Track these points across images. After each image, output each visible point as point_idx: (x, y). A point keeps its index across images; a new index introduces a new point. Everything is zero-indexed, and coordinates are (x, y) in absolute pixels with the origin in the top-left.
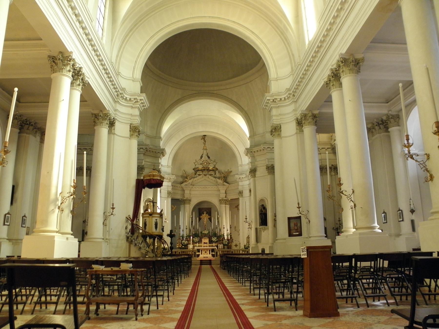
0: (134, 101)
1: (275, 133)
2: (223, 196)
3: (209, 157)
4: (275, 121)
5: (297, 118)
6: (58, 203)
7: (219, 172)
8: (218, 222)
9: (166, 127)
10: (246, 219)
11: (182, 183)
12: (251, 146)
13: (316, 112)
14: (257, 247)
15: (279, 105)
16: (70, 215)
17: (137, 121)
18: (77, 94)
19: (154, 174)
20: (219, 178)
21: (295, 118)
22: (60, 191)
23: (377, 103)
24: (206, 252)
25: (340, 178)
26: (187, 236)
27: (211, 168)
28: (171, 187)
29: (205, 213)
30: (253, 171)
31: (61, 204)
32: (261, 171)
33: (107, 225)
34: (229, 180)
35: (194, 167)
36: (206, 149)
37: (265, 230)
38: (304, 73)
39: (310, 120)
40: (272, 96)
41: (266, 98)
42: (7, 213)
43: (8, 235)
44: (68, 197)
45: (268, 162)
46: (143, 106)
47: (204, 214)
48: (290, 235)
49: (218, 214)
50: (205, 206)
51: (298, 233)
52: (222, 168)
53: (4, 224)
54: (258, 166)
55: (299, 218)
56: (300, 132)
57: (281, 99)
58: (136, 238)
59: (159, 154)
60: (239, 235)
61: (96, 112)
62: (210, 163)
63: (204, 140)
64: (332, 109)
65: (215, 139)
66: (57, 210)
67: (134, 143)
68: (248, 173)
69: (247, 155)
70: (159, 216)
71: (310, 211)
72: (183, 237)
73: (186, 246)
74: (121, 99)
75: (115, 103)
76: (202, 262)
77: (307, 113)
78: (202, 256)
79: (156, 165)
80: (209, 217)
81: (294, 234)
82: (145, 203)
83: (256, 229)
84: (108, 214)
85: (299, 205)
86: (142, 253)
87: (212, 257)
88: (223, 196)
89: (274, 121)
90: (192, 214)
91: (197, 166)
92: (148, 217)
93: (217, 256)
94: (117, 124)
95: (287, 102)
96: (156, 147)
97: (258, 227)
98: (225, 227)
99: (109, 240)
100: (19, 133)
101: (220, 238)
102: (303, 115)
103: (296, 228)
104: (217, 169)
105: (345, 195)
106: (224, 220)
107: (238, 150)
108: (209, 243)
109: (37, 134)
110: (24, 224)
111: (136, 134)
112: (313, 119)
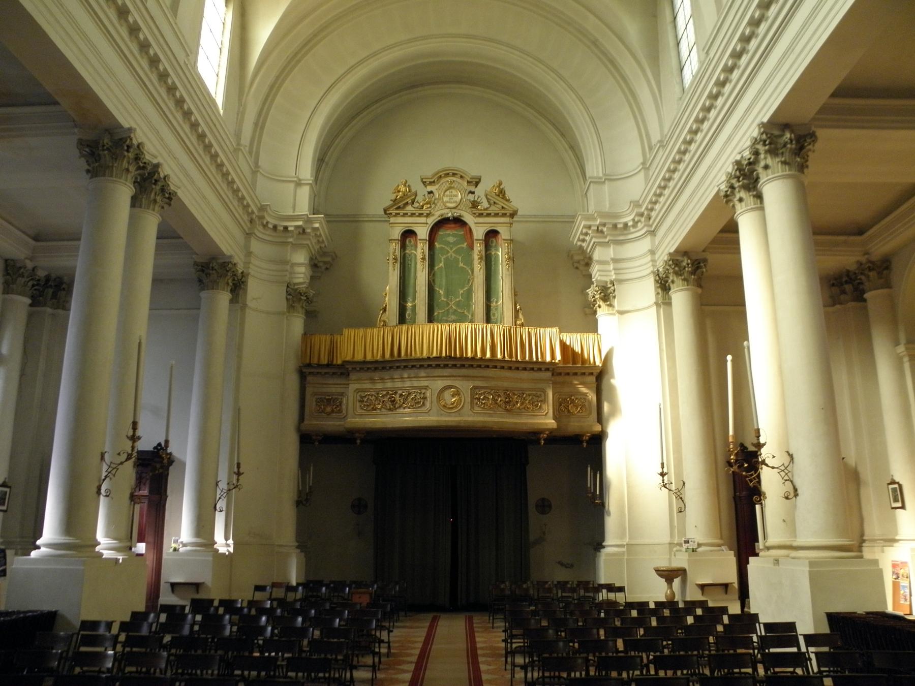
18: (151, 222)
38: (667, 176)
71: (127, 495)
85: (663, 467)
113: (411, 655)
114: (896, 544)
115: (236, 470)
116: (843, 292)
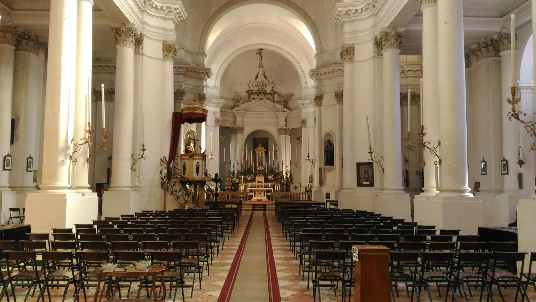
0: (167, 11)
1: (346, 57)
2: (282, 124)
3: (266, 77)
4: (348, 40)
5: (376, 37)
6: (69, 152)
7: (279, 95)
8: (276, 155)
9: (212, 38)
10: (308, 156)
12: (318, 68)
13: (401, 30)
14: (320, 191)
15: (353, 18)
16: (87, 165)
17: (172, 37)
19: (195, 106)
20: (278, 103)
21: (373, 37)
22: (71, 137)
23: (476, 17)
24: (260, 194)
25: (423, 126)
27: (268, 90)
29: (260, 145)
30: (319, 99)
31: (73, 153)
32: (329, 99)
33: (137, 170)
34: (291, 104)
35: (248, 89)
36: (263, 67)
37: (330, 170)
39: (392, 41)
40: (345, 7)
41: (337, 8)
42: (6, 154)
43: (10, 182)
44: (83, 144)
45: (338, 87)
46: (179, 17)
48: (359, 184)
49: (276, 146)
51: (368, 183)
52: (282, 90)
53: (4, 169)
54: (325, 92)
55: (371, 164)
56: (379, 55)
57: (356, 11)
58: (172, 184)
59: (203, 75)
60: (300, 173)
61: (116, 25)
62: (266, 85)
63: (260, 55)
64: (422, 26)
65: (274, 54)
66: (68, 161)
67: (170, 66)
68: (313, 98)
69: (311, 78)
70: (201, 158)
71: (385, 158)
72: (233, 174)
73: (236, 186)
74: (149, 7)
75: (141, 13)
76: (255, 207)
77: (389, 31)
78: (255, 199)
81: (364, 183)
82: (187, 136)
83: (320, 169)
84: (138, 157)
86: (180, 203)
88: (282, 124)
89: (346, 40)
90: (245, 146)
91: (251, 88)
92: (188, 159)
93: (272, 200)
94: (146, 41)
95: (365, 15)
96: (199, 65)
97: (323, 167)
98: (284, 162)
99: (139, 187)
100: (16, 50)
101: (278, 175)
102: (383, 34)
103: (366, 176)
104: (276, 92)
105: (428, 148)
106: (283, 154)
107: (302, 69)
108: (265, 182)
109: (41, 51)
110: (30, 167)
111: (171, 54)
112: (397, 40)
113: (234, 249)
114: (502, 194)
115: (142, 148)
116: (488, 51)
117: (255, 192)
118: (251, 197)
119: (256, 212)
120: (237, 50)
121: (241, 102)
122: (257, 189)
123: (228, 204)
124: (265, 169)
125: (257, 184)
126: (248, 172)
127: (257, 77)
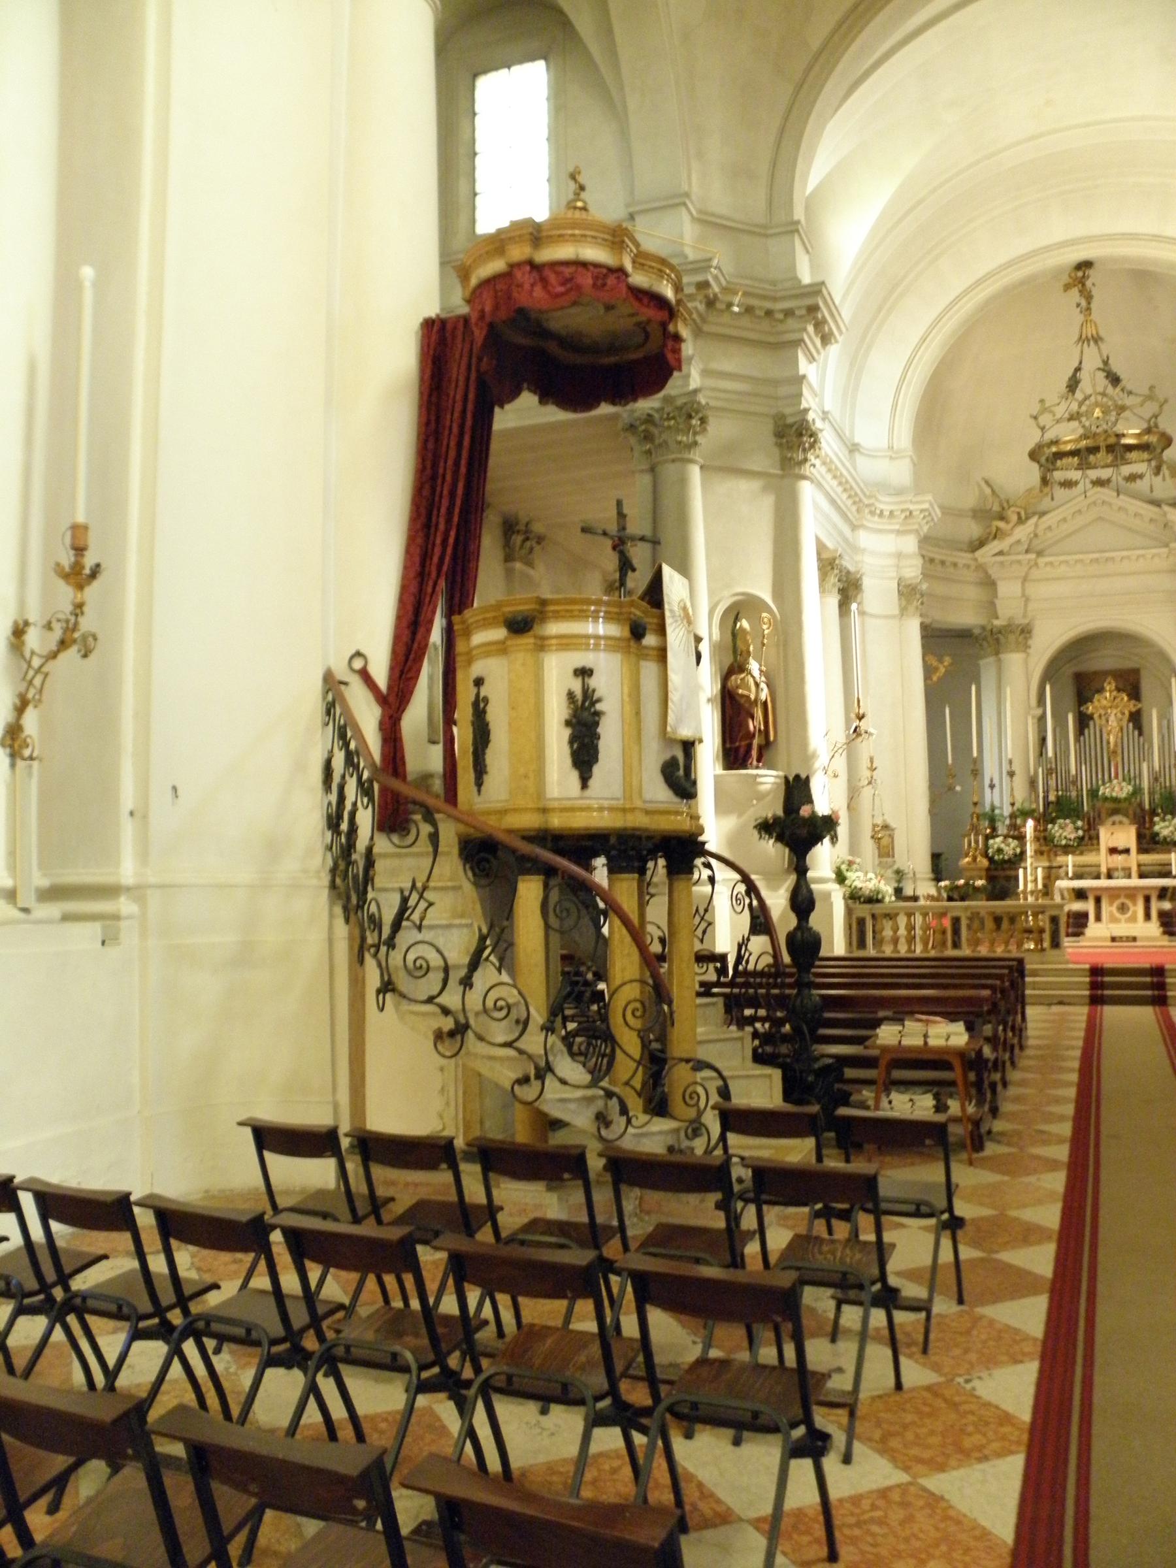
11: (981, 543)
24: (1123, 908)
26: (1013, 816)
27: (1131, 433)
28: (919, 562)
36: (1097, 339)
47: (1100, 690)
50: (1106, 660)
59: (791, 323)
62: (1122, 409)
72: (992, 820)
76: (1103, 985)
79: (783, 391)
80: (1132, 706)
87: (1165, 941)
91: (1050, 435)
92: (501, 649)
108: (1142, 850)
117: (1098, 901)
118: (1079, 922)
119: (1110, 1013)
120: (978, 282)
121: (1014, 518)
122: (1103, 883)
123: (902, 1011)
124: (1137, 791)
125: (1103, 860)
126: (1062, 808)
127: (1073, 385)
